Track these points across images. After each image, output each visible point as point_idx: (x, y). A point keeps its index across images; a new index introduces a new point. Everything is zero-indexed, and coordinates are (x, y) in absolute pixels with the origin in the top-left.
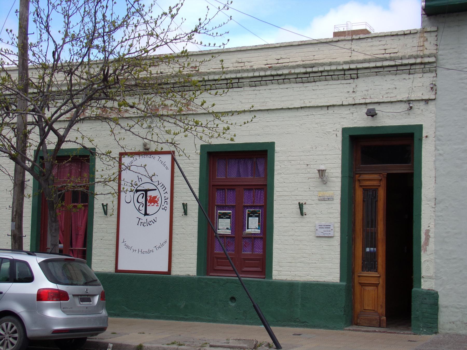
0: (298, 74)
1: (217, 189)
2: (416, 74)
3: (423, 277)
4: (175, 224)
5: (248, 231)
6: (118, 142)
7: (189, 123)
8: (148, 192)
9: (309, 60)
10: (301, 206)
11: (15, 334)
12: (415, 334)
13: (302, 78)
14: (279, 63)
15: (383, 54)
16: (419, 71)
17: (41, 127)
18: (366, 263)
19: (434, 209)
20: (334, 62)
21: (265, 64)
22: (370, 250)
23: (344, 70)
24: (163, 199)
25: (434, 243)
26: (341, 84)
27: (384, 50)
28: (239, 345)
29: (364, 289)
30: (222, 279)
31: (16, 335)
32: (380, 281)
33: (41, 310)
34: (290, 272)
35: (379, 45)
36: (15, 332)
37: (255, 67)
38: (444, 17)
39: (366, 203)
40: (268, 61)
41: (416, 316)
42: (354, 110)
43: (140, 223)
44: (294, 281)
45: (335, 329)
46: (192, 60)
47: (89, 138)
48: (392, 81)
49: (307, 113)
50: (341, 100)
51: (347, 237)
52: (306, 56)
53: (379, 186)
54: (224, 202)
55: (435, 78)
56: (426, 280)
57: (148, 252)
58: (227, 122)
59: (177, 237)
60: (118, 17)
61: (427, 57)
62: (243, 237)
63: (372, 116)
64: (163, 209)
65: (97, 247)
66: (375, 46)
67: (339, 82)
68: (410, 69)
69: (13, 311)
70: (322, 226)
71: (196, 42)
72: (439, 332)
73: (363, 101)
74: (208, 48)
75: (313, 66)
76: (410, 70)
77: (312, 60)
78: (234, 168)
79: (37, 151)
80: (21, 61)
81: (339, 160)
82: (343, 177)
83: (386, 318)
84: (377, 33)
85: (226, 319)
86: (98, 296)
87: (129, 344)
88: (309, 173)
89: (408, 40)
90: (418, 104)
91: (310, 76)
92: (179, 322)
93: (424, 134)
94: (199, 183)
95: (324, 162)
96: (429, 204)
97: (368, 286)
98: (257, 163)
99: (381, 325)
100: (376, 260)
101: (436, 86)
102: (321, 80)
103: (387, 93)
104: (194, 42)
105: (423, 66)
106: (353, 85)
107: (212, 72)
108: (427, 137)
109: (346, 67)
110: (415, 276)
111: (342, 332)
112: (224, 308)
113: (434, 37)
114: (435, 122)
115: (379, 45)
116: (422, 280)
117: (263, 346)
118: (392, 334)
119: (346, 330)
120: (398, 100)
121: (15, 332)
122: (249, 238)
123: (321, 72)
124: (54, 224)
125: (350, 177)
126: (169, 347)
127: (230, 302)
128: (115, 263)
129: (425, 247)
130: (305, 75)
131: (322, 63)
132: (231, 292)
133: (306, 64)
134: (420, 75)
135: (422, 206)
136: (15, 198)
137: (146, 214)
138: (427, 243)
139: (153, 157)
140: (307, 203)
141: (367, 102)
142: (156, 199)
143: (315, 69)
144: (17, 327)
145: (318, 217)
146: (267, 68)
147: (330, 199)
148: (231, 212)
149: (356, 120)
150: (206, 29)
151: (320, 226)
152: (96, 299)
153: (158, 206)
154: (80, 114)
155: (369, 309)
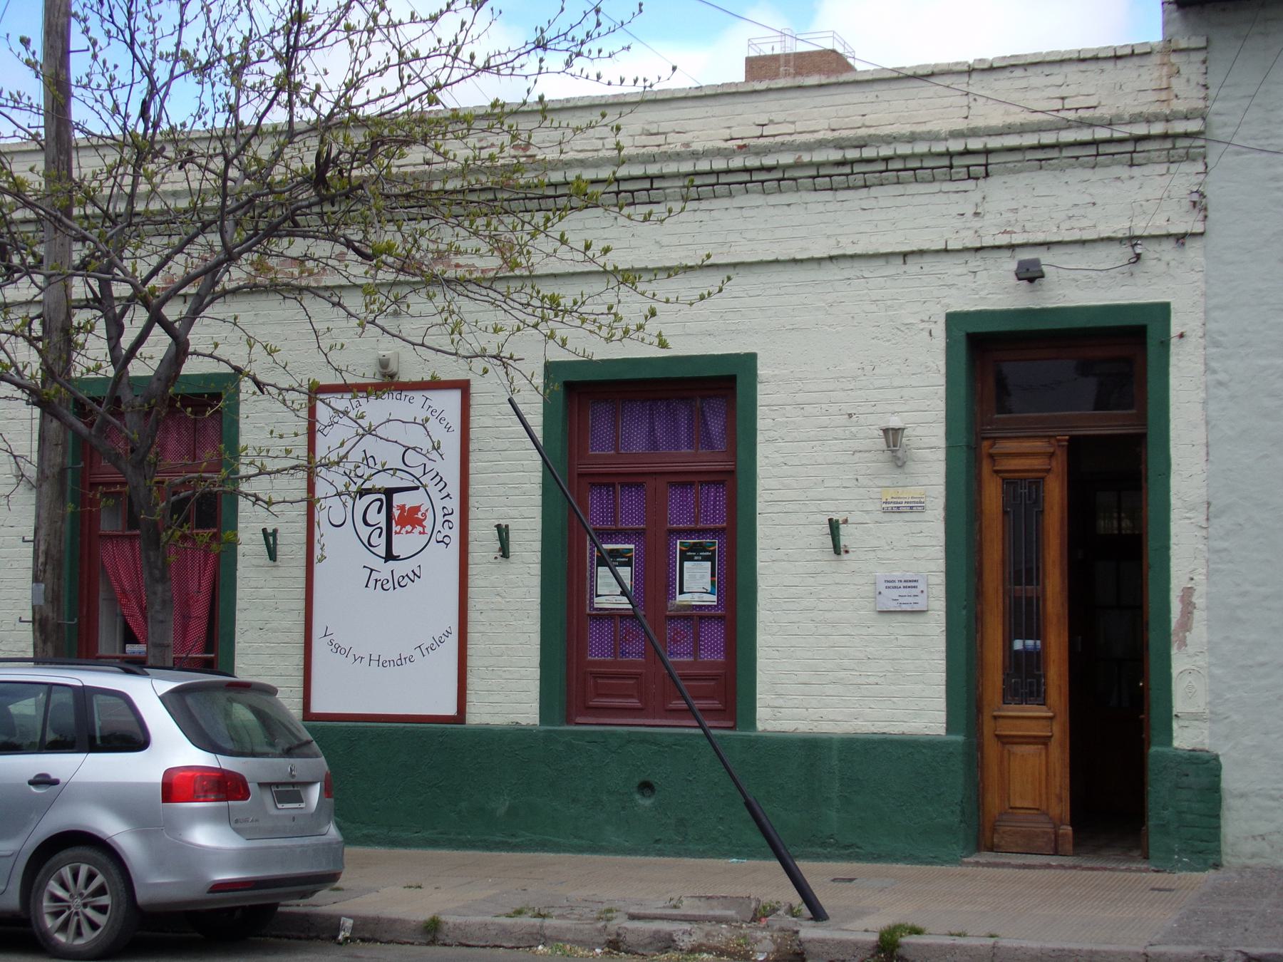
0: (819, 165)
1: (593, 484)
2: (1150, 165)
3: (1176, 716)
4: (473, 582)
5: (681, 599)
6: (326, 355)
7: (531, 303)
8: (395, 495)
9: (851, 128)
10: (834, 527)
11: (101, 895)
12: (1158, 871)
13: (830, 176)
14: (764, 134)
15: (1058, 111)
16: (1159, 157)
17: (110, 315)
18: (1013, 680)
19: (1204, 533)
20: (923, 132)
21: (725, 138)
22: (1024, 645)
23: (949, 154)
24: (439, 514)
25: (1205, 622)
26: (941, 194)
27: (1060, 101)
28: (711, 913)
29: (1009, 751)
30: (613, 734)
31: (105, 900)
32: (1054, 728)
33: (173, 827)
34: (807, 709)
35: (1047, 87)
36: (101, 891)
37: (697, 146)
38: (1224, 10)
39: (1012, 518)
40: (733, 129)
41: (1161, 822)
42: (978, 263)
43: (372, 583)
44: (818, 735)
45: (937, 864)
46: (556, 124)
47: (267, 345)
48: (1085, 183)
49: (846, 274)
50: (943, 236)
51: (964, 612)
52: (843, 115)
53: (1048, 471)
54: (611, 521)
55: (1202, 176)
56: (1186, 723)
57: (399, 662)
58: (654, 295)
59: (481, 618)
60: (315, 5)
61: (1181, 119)
62: (666, 616)
63: (1031, 280)
64: (438, 542)
65: (249, 652)
66: (1033, 89)
67: (935, 187)
68: (1134, 152)
69: (95, 833)
70: (894, 581)
71: (584, 75)
72: (1224, 863)
73: (1003, 240)
74: (616, 90)
75: (863, 143)
76: (1135, 155)
77: (859, 128)
78: (638, 425)
79: (115, 381)
80: (53, 129)
81: (939, 401)
82: (950, 448)
83: (1074, 831)
84: (1041, 53)
85: (627, 844)
86: (319, 784)
87: (402, 916)
88: (854, 437)
89: (1127, 73)
90: (1158, 248)
91: (855, 172)
92: (494, 853)
93: (1175, 329)
94: (541, 470)
95: (896, 408)
96: (1190, 518)
97: (1022, 743)
98: (703, 412)
99: (1060, 849)
100: (1042, 672)
101: (1205, 197)
102: (885, 182)
103: (1070, 218)
104: (579, 73)
105: (1168, 144)
106: (976, 196)
107: (577, 160)
108: (1181, 336)
109: (955, 146)
110: (1155, 712)
111: (958, 869)
112: (622, 812)
113: (1199, 65)
114: (1204, 295)
115: (1047, 87)
116: (1175, 725)
117: (778, 912)
118: (1095, 873)
119: (969, 863)
120: (1102, 236)
121: (101, 891)
122: (687, 619)
123: (886, 159)
124: (159, 588)
125: (969, 447)
126: (516, 923)
127: (637, 796)
128: (301, 695)
129: (1181, 635)
130: (840, 167)
131: (889, 136)
132: (642, 768)
133: (843, 139)
134: (1162, 168)
135: (1172, 524)
136: (44, 514)
137: (390, 556)
138: (1186, 625)
139: (407, 398)
140: (850, 521)
141: (1014, 242)
142: (420, 514)
143: (868, 153)
144: (104, 875)
145: (881, 559)
146: (734, 150)
147: (915, 508)
148: (632, 546)
149: (986, 292)
150: (573, 40)
151: (888, 582)
152: (315, 793)
153: (424, 533)
154: (222, 276)
155: (1026, 806)
